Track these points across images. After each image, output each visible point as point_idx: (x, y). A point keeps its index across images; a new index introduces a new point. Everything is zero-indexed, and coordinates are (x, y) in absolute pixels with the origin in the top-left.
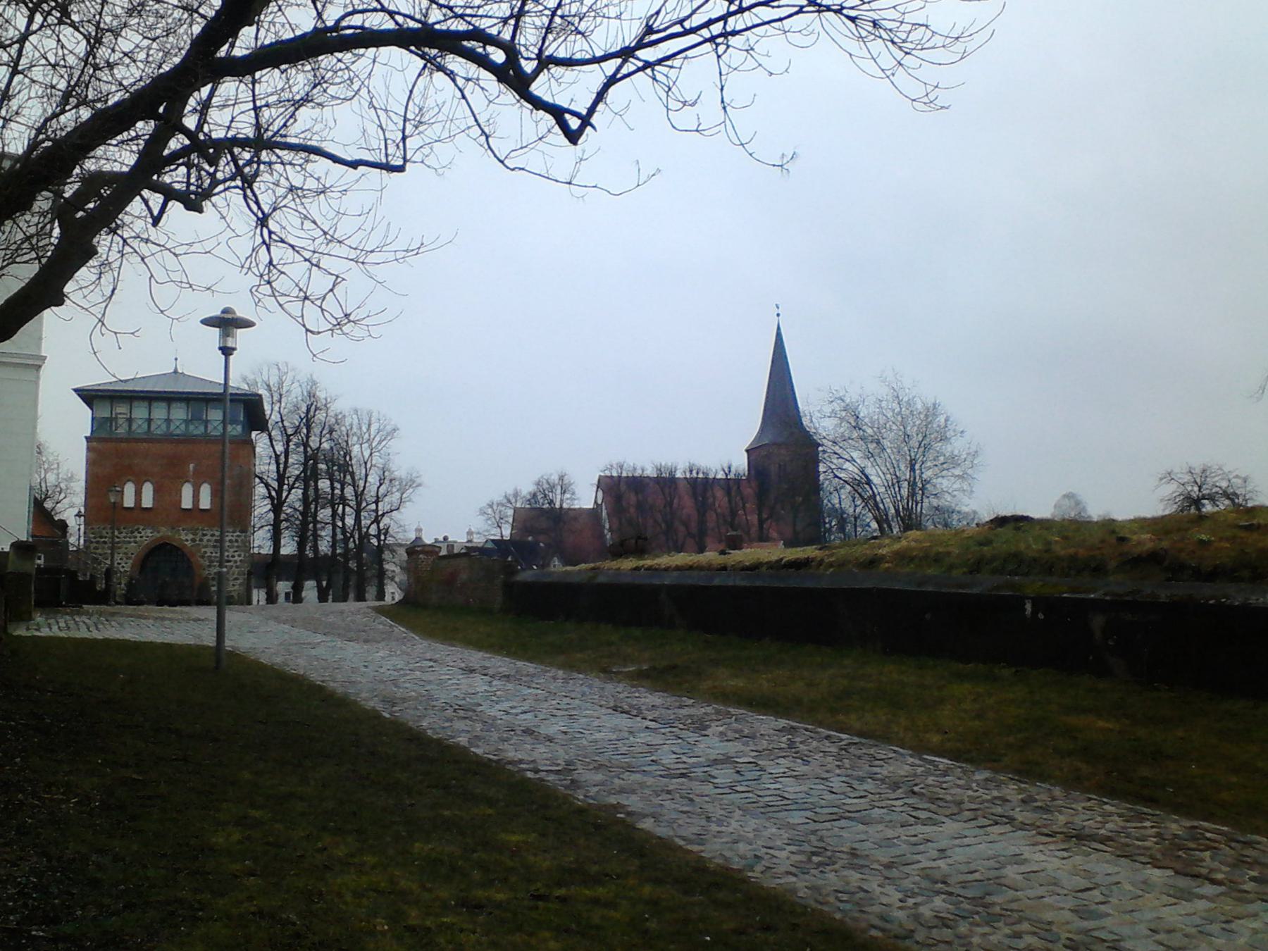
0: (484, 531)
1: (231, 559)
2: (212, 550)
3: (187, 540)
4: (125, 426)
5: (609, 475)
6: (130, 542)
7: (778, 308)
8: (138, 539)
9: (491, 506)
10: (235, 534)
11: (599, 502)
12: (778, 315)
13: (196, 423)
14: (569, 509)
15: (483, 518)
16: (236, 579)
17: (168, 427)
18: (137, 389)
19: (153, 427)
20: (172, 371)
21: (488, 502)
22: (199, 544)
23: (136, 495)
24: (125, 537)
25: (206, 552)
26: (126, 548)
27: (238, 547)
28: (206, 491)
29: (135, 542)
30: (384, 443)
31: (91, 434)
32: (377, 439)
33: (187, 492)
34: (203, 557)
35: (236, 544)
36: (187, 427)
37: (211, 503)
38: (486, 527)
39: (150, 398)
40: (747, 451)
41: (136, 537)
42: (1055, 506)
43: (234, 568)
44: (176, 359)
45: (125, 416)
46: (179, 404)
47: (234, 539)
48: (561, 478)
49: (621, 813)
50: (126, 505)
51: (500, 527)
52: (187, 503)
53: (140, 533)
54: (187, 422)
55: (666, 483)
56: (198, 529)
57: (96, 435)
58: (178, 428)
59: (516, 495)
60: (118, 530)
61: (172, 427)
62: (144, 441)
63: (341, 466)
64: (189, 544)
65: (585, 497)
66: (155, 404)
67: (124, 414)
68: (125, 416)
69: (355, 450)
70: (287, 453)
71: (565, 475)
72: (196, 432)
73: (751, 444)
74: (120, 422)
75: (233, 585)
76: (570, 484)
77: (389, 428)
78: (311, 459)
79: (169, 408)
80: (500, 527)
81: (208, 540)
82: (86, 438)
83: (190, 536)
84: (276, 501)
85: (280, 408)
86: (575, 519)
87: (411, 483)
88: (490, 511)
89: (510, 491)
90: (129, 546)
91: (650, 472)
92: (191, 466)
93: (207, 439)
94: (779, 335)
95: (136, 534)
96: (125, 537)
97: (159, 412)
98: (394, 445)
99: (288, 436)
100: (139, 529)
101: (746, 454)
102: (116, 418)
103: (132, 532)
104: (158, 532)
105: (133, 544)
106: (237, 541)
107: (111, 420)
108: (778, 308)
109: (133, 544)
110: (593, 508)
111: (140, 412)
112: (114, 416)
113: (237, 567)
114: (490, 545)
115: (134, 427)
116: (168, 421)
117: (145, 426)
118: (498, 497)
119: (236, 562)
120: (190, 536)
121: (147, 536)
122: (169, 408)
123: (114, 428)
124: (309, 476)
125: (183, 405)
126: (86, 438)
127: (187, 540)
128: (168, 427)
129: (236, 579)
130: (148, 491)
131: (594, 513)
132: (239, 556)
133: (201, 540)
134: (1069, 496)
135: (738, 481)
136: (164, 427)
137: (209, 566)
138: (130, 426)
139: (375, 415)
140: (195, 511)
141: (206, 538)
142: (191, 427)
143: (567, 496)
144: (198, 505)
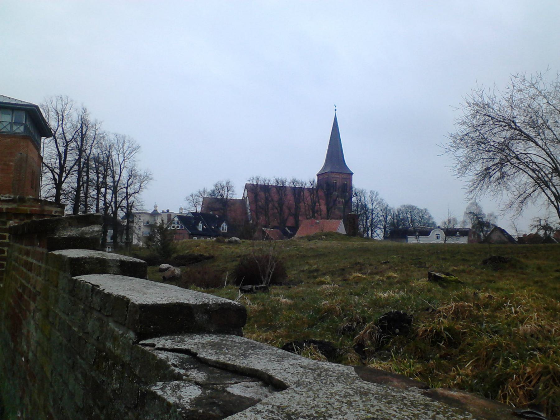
5: (252, 183)
7: (336, 106)
12: (336, 110)
15: (187, 202)
21: (190, 194)
38: (189, 206)
40: (318, 175)
42: (467, 209)
48: (228, 183)
51: (196, 207)
55: (280, 189)
59: (204, 191)
65: (239, 193)
71: (230, 182)
73: (319, 172)
80: (196, 207)
89: (202, 190)
91: (273, 183)
108: (336, 106)
110: (242, 199)
118: (196, 192)
131: (243, 201)
135: (301, 189)
139: (127, 138)
143: (230, 192)
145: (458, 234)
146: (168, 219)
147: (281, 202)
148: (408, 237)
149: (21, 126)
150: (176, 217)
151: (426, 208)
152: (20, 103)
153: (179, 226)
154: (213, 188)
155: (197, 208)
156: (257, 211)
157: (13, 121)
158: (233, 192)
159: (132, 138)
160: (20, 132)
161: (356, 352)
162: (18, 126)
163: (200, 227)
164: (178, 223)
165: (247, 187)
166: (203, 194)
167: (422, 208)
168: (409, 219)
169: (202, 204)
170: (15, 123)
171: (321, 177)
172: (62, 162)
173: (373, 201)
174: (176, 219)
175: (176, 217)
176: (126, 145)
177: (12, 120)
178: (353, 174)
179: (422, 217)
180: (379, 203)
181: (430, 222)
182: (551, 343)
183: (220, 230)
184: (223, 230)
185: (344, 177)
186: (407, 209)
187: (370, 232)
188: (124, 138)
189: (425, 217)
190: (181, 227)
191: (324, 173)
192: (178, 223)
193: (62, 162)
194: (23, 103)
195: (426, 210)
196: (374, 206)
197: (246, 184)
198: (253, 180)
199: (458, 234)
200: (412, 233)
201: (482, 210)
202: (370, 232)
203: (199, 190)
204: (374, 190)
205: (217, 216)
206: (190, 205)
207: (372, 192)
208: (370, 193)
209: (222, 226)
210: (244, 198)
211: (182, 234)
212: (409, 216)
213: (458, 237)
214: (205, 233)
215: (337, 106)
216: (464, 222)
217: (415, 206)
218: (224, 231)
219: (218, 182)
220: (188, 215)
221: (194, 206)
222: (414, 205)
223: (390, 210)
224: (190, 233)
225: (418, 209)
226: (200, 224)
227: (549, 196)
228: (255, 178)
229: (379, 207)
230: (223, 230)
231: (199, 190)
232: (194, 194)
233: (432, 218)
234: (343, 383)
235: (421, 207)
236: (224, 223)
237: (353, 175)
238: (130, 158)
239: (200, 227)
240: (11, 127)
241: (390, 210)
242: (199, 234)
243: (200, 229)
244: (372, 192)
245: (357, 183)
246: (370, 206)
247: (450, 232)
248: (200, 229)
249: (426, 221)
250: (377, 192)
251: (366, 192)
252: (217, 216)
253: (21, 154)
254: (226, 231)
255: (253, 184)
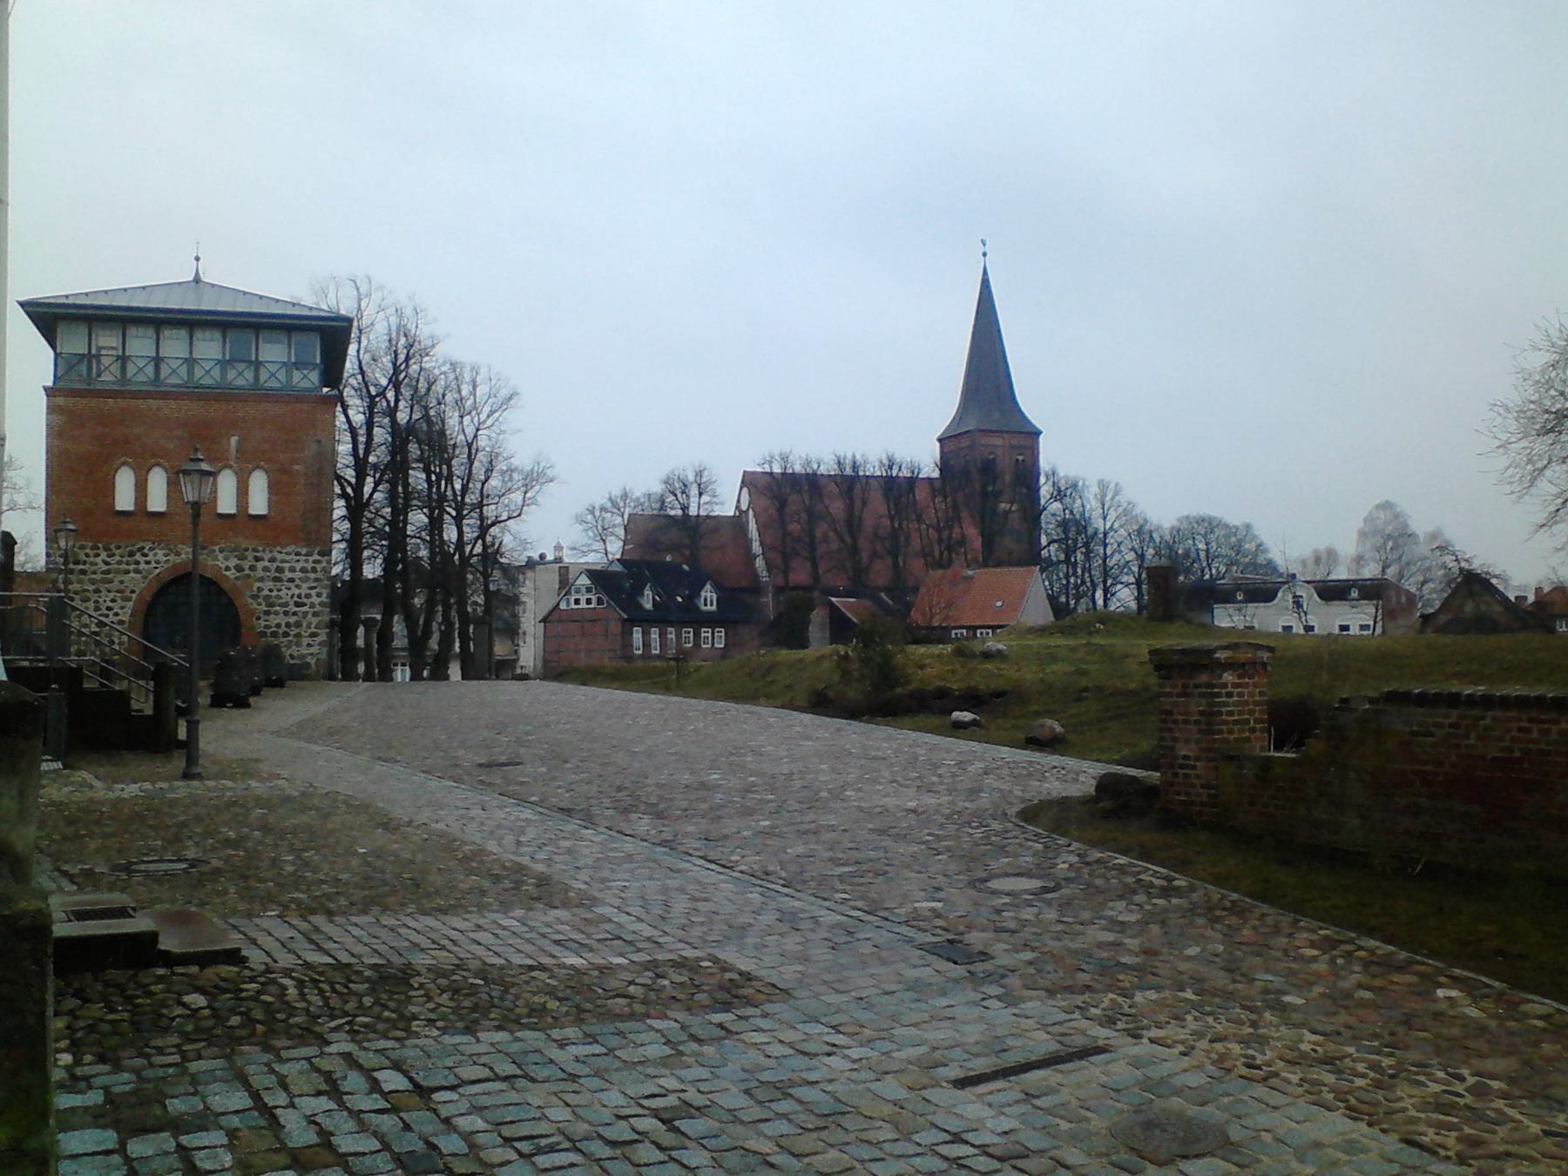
0: (583, 546)
1: (305, 600)
2: (270, 584)
3: (227, 569)
4: (116, 368)
5: (768, 470)
6: (127, 572)
7: (984, 245)
8: (142, 566)
9: (592, 512)
10: (311, 559)
11: (744, 507)
12: (985, 254)
13: (241, 367)
14: (708, 517)
15: (580, 528)
16: (313, 635)
17: (190, 372)
18: (134, 304)
19: (165, 371)
20: (191, 279)
21: (587, 506)
22: (248, 576)
23: (136, 491)
24: (119, 563)
25: (260, 590)
26: (122, 582)
27: (316, 580)
28: (259, 486)
29: (137, 571)
30: (496, 415)
31: (54, 383)
32: (487, 409)
33: (226, 486)
34: (255, 597)
35: (313, 576)
36: (223, 373)
37: (136, 504)
38: (585, 540)
39: (158, 321)
40: (940, 440)
41: (137, 563)
42: (1365, 520)
43: (310, 616)
44: (197, 259)
45: (114, 352)
46: (208, 333)
47: (309, 566)
48: (699, 474)
49: (534, 795)
50: (119, 507)
51: (604, 541)
52: (226, 503)
53: (146, 555)
54: (224, 364)
55: (850, 482)
56: (246, 550)
57: (61, 384)
58: (205, 373)
59: (625, 496)
60: (106, 549)
61: (198, 373)
62: (146, 395)
63: (436, 445)
64: (231, 574)
65: (726, 500)
66: (167, 333)
67: (112, 348)
68: (114, 352)
69: (452, 421)
70: (370, 424)
71: (705, 469)
72: (240, 382)
73: (942, 434)
74: (105, 361)
75: (309, 645)
76: (710, 482)
77: (504, 393)
78: (401, 437)
79: (191, 338)
80: (604, 541)
81: (266, 569)
82: (46, 389)
83: (233, 562)
84: (353, 503)
85: (358, 351)
86: (715, 530)
87: (534, 479)
88: (590, 517)
89: (617, 492)
90: (126, 578)
91: (827, 467)
92: (234, 440)
93: (259, 394)
94: (985, 284)
95: (138, 557)
96: (119, 563)
97: (174, 345)
98: (511, 418)
99: (372, 398)
100: (143, 548)
101: (938, 444)
102: (98, 356)
103: (131, 554)
104: (178, 554)
105: (132, 575)
106: (314, 570)
107: (90, 358)
108: (984, 245)
109: (132, 575)
110: (734, 516)
111: (140, 344)
112: (94, 351)
113: (315, 614)
114: (617, 568)
115: (131, 370)
116: (191, 362)
117: (150, 370)
118: (600, 500)
119: (312, 606)
120: (233, 562)
121: (160, 561)
122: (191, 338)
123: (94, 376)
124: (397, 468)
125: (217, 335)
126: (46, 389)
127: (227, 569)
128: (190, 372)
129: (313, 635)
130: (158, 483)
131: (738, 522)
132: (319, 595)
133: (252, 568)
134: (1386, 506)
136: (183, 371)
137: (267, 613)
138: (124, 369)
139: (483, 373)
140: (241, 520)
141: (260, 565)
142: (231, 374)
143: (705, 498)
144: (146, 507)
145: (1355, 594)
146: (560, 582)
147: (852, 524)
148: (1215, 606)
149: (314, 369)
150: (583, 576)
151: (1248, 521)
152: (306, 313)
153: (594, 599)
154: (657, 488)
155: (608, 544)
156: (782, 550)
157: (293, 360)
158: (714, 496)
159: (498, 373)
160: (310, 385)
161: (1488, 581)
162: (306, 372)
163: (647, 600)
164: (589, 590)
165: (749, 480)
166: (622, 504)
167: (1237, 523)
168: (1202, 554)
169: (626, 536)
170: (298, 365)
171: (951, 446)
172: (361, 447)
173: (1106, 508)
174: (584, 581)
175: (583, 576)
176: (482, 391)
177: (289, 358)
178: (1041, 433)
179: (1238, 548)
180: (1125, 511)
181: (1261, 560)
182: (1415, 565)
183: (698, 608)
184: (706, 605)
185: (1015, 442)
186: (1196, 526)
187: (1099, 594)
188: (475, 370)
189: (1247, 546)
190: (600, 601)
191: (960, 434)
192: (589, 590)
193: (361, 447)
194: (314, 313)
195: (1248, 527)
196: (1108, 525)
197: (745, 472)
198: (771, 462)
199: (1355, 594)
200: (1226, 597)
201: (1410, 523)
202: (1099, 594)
203: (610, 493)
204: (1107, 478)
205: (686, 567)
206: (590, 538)
207: (1103, 485)
208: (1097, 489)
209: (703, 594)
210: (741, 512)
211: (599, 620)
212: (1202, 546)
213: (1354, 602)
214: (660, 618)
215: (987, 244)
216: (1359, 560)
217: (1216, 518)
218: (709, 607)
219: (673, 472)
220: (610, 569)
221: (599, 538)
222: (1213, 513)
223: (1151, 532)
224: (626, 617)
225: (1226, 526)
226: (648, 592)
227: (987, 1091)
228: (777, 458)
229: (1121, 526)
230: (706, 605)
231: (610, 493)
232: (597, 507)
233: (1266, 551)
234: (957, 1139)
235: (1234, 518)
236: (708, 587)
237: (1041, 438)
238: (493, 425)
239: (647, 600)
240: (289, 376)
241: (1151, 532)
242: (646, 620)
243: (649, 606)
244: (1103, 485)
245: (1055, 457)
246: (1098, 524)
247: (1332, 592)
248: (649, 606)
249: (1250, 557)
250: (1117, 485)
251: (1087, 483)
252: (686, 567)
253: (320, 442)
254: (714, 608)
255: (771, 474)
